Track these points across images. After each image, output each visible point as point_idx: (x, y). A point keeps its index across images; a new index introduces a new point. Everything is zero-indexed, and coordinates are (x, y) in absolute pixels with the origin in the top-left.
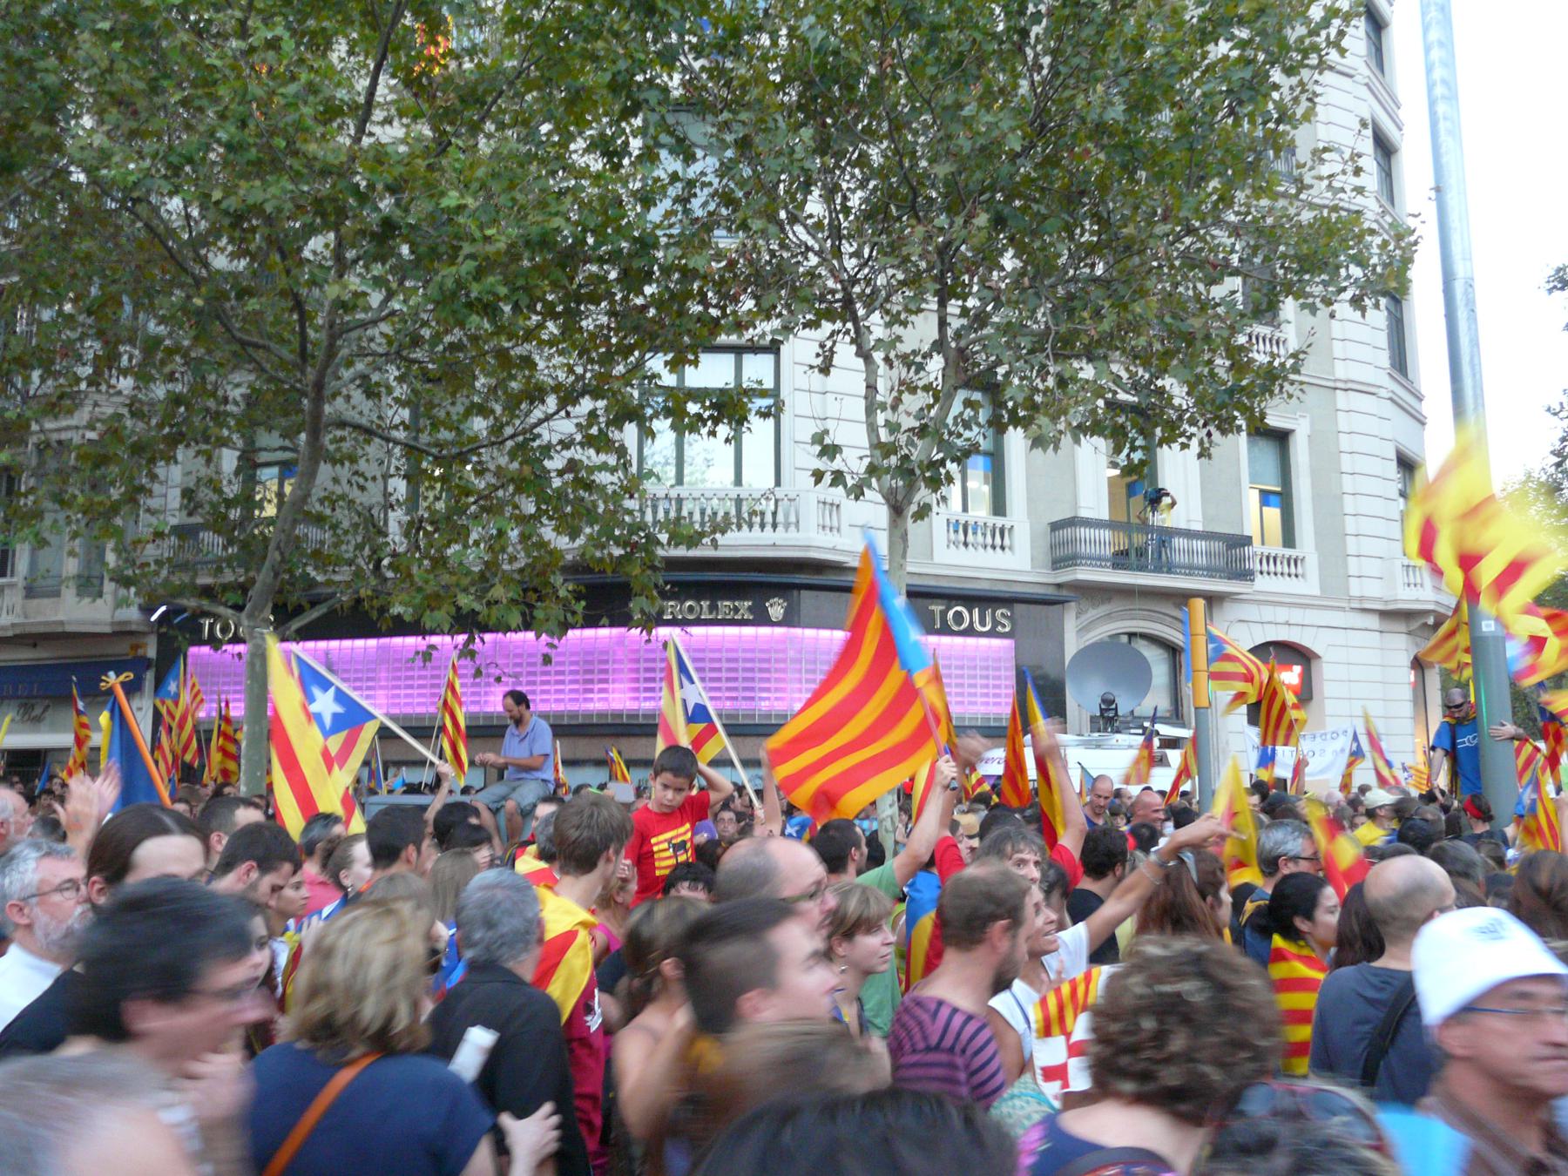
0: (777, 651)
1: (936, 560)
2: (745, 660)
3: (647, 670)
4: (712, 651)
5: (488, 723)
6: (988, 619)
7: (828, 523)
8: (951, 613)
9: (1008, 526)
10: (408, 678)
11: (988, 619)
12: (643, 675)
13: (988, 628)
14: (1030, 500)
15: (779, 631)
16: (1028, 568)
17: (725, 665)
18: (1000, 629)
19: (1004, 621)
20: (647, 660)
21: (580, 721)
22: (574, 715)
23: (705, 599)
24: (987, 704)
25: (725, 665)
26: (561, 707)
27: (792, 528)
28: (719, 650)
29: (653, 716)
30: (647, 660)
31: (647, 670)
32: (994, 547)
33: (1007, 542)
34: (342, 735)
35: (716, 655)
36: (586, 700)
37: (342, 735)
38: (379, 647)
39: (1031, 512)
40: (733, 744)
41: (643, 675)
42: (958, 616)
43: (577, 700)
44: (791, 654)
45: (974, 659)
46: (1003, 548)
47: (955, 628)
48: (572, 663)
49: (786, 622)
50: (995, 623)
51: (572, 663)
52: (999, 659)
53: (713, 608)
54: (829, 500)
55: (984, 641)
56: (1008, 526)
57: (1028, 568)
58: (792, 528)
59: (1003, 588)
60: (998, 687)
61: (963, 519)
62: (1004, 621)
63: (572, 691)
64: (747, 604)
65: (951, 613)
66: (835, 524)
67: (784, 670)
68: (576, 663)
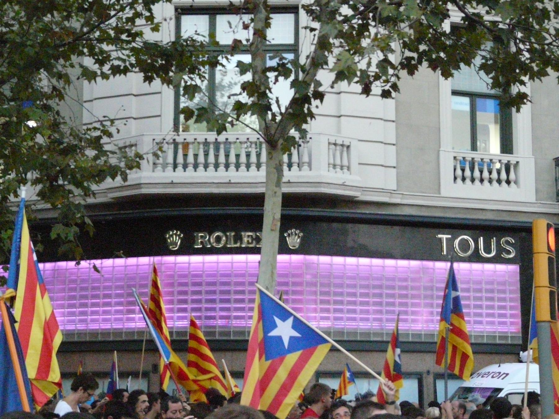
0: (294, 276)
1: (444, 193)
2: (208, 284)
3: (180, 293)
4: (237, 275)
5: (130, 338)
6: (493, 246)
7: (338, 162)
8: (457, 242)
9: (513, 162)
10: (82, 297)
11: (493, 246)
12: (177, 297)
13: (493, 254)
14: (535, 138)
15: (296, 258)
16: (534, 200)
17: (191, 288)
18: (505, 255)
19: (508, 248)
20: (180, 284)
21: (124, 338)
22: (118, 332)
23: (231, 231)
24: (492, 323)
25: (191, 288)
26: (107, 326)
27: (306, 167)
28: (243, 275)
29: (242, 333)
30: (180, 284)
31: (180, 293)
32: (499, 181)
33: (512, 176)
34: (298, 354)
35: (240, 280)
36: (129, 320)
37: (298, 354)
38: (54, 270)
39: (537, 148)
40: (213, 355)
41: (177, 297)
42: (464, 246)
43: (121, 320)
44: (308, 278)
45: (480, 282)
46: (508, 182)
47: (462, 255)
48: (118, 287)
49: (303, 250)
50: (500, 250)
51: (118, 287)
52: (504, 283)
53: (238, 238)
54: (339, 142)
55: (489, 267)
56: (513, 162)
57: (534, 200)
58: (306, 167)
59: (507, 218)
60: (504, 308)
61: (470, 155)
62: (508, 248)
63: (117, 312)
64: (233, 234)
65: (457, 242)
66: (345, 163)
67: (300, 293)
68: (121, 287)
